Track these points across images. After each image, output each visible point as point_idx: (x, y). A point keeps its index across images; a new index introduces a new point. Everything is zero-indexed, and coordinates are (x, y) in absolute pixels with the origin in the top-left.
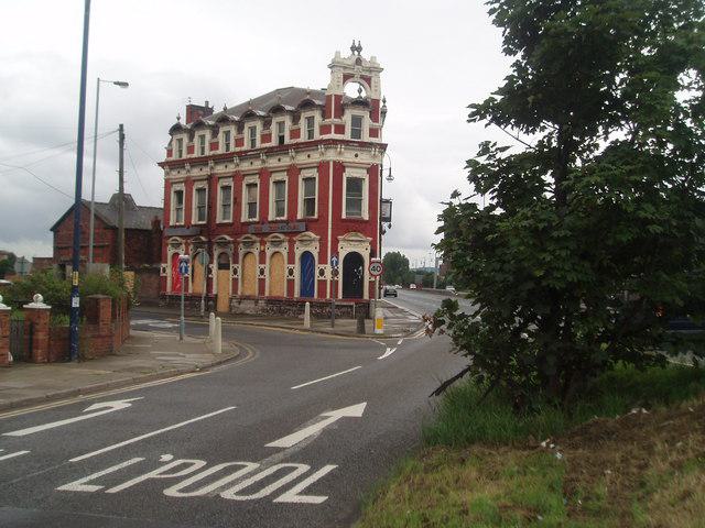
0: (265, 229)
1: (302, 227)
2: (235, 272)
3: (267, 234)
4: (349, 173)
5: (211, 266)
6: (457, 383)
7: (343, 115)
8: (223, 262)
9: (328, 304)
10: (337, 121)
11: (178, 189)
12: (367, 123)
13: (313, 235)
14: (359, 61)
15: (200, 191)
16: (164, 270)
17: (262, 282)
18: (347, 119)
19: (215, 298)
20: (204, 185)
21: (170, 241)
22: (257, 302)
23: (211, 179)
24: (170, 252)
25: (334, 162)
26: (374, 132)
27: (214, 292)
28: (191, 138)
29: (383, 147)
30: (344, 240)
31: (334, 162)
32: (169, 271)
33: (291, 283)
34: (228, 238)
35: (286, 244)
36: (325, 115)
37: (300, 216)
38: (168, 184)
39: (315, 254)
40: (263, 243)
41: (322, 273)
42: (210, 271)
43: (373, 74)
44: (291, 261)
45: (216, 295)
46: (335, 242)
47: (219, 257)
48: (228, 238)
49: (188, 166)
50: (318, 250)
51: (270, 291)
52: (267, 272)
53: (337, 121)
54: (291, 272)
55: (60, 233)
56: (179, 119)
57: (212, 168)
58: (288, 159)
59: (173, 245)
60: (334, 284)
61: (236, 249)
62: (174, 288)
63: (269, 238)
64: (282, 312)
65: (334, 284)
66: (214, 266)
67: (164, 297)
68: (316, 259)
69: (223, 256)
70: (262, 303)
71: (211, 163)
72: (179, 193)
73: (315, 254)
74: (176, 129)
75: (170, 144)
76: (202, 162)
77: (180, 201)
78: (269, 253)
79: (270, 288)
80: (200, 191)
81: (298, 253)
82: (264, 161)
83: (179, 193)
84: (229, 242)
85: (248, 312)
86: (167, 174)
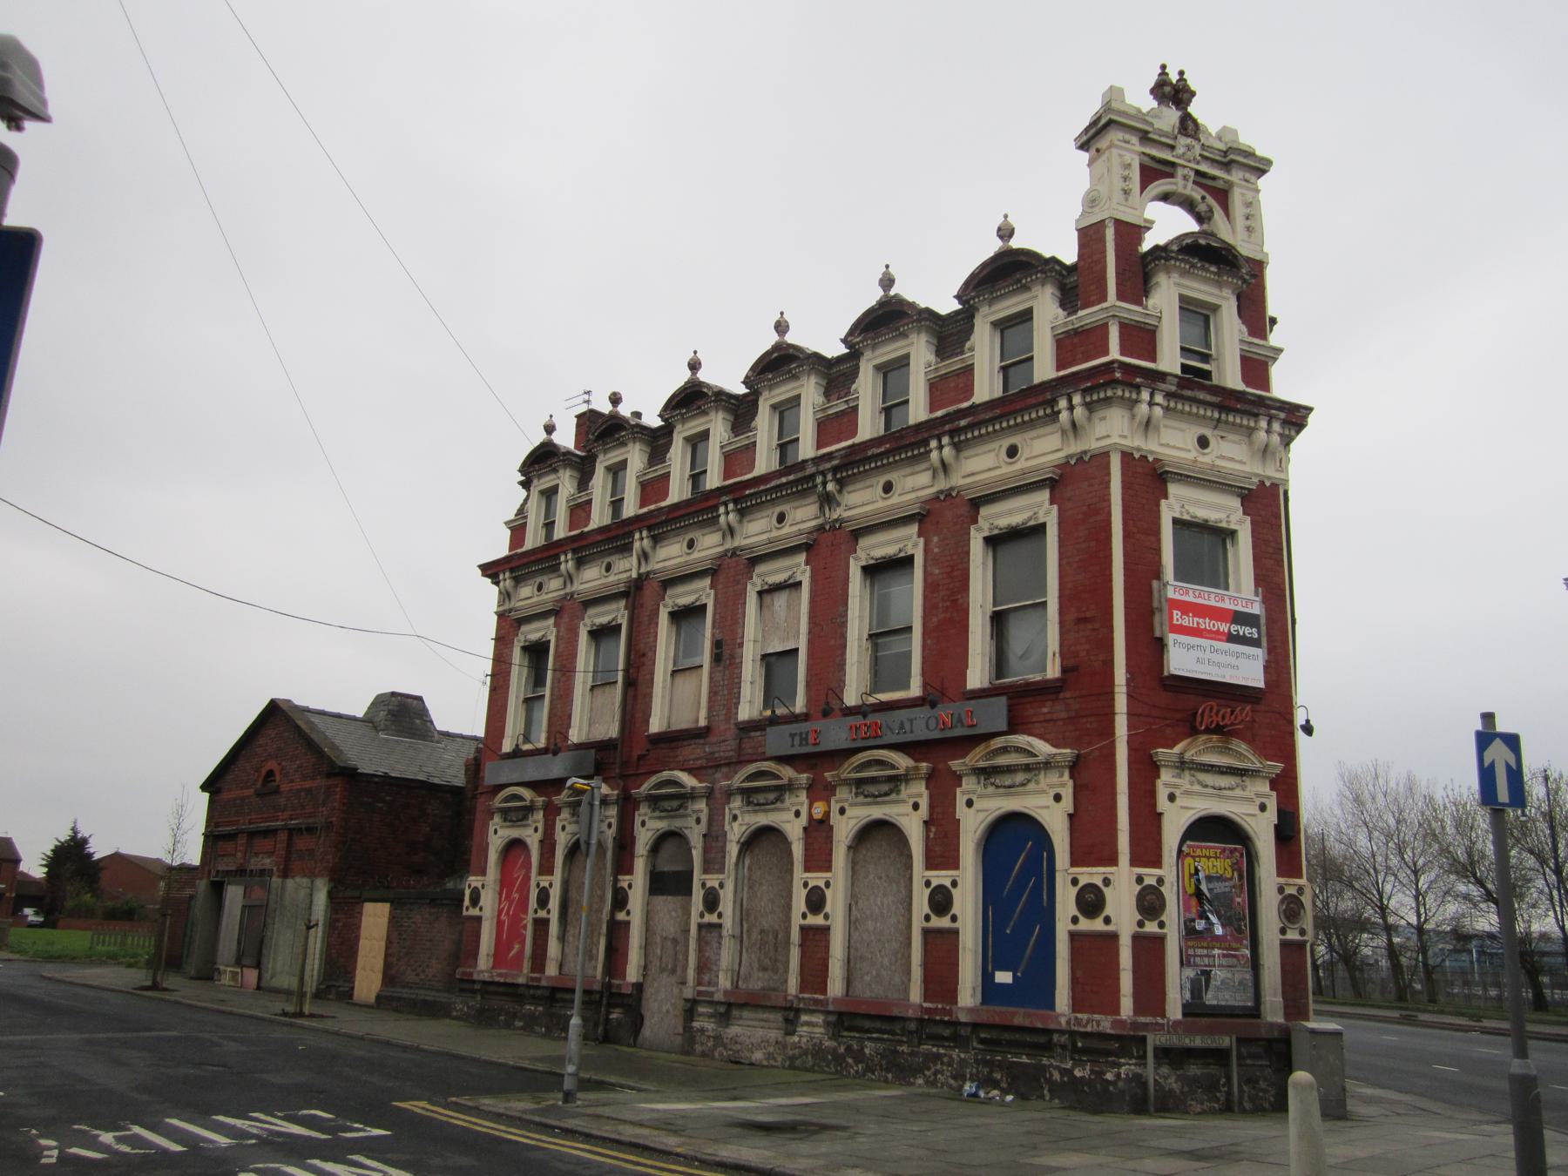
0: (836, 734)
1: (995, 714)
2: (711, 902)
3: (840, 755)
4: (1179, 503)
5: (624, 881)
6: (410, 700)
7: (1146, 293)
8: (666, 866)
9: (1129, 1042)
10: (1131, 311)
11: (534, 637)
12: (1230, 331)
13: (1043, 748)
14: (1189, 126)
15: (601, 634)
16: (475, 900)
17: (815, 938)
18: (1165, 297)
19: (633, 1002)
20: (616, 613)
21: (498, 801)
22: (790, 1025)
23: (634, 592)
24: (498, 835)
25: (1127, 456)
26: (1256, 368)
27: (632, 974)
28: (584, 482)
29: (1295, 417)
30: (1182, 765)
31: (1127, 456)
32: (488, 900)
33: (941, 945)
34: (688, 780)
35: (919, 791)
36: (1070, 298)
37: (977, 675)
38: (509, 623)
39: (1055, 821)
40: (819, 791)
41: (1091, 901)
42: (620, 900)
43: (1236, 176)
44: (942, 853)
45: (639, 987)
46: (1145, 771)
47: (655, 848)
48: (688, 780)
49: (567, 563)
50: (1067, 804)
51: (849, 981)
52: (836, 902)
53: (1131, 311)
54: (941, 901)
55: (224, 796)
56: (550, 429)
57: (645, 556)
58: (923, 478)
59: (505, 813)
60: (1149, 949)
61: (715, 820)
62: (499, 956)
63: (847, 770)
64: (899, 1070)
65: (1149, 949)
66: (637, 882)
67: (467, 986)
68: (798, 850)
69: (669, 848)
70: (812, 1028)
71: (641, 542)
72: (536, 652)
73: (1055, 821)
74: (542, 459)
75: (521, 511)
76: (617, 537)
77: (538, 681)
78: (844, 829)
79: (849, 962)
80: (601, 634)
81: (972, 823)
82: (827, 500)
83: (536, 652)
84: (692, 796)
85: (758, 1056)
86: (505, 596)
